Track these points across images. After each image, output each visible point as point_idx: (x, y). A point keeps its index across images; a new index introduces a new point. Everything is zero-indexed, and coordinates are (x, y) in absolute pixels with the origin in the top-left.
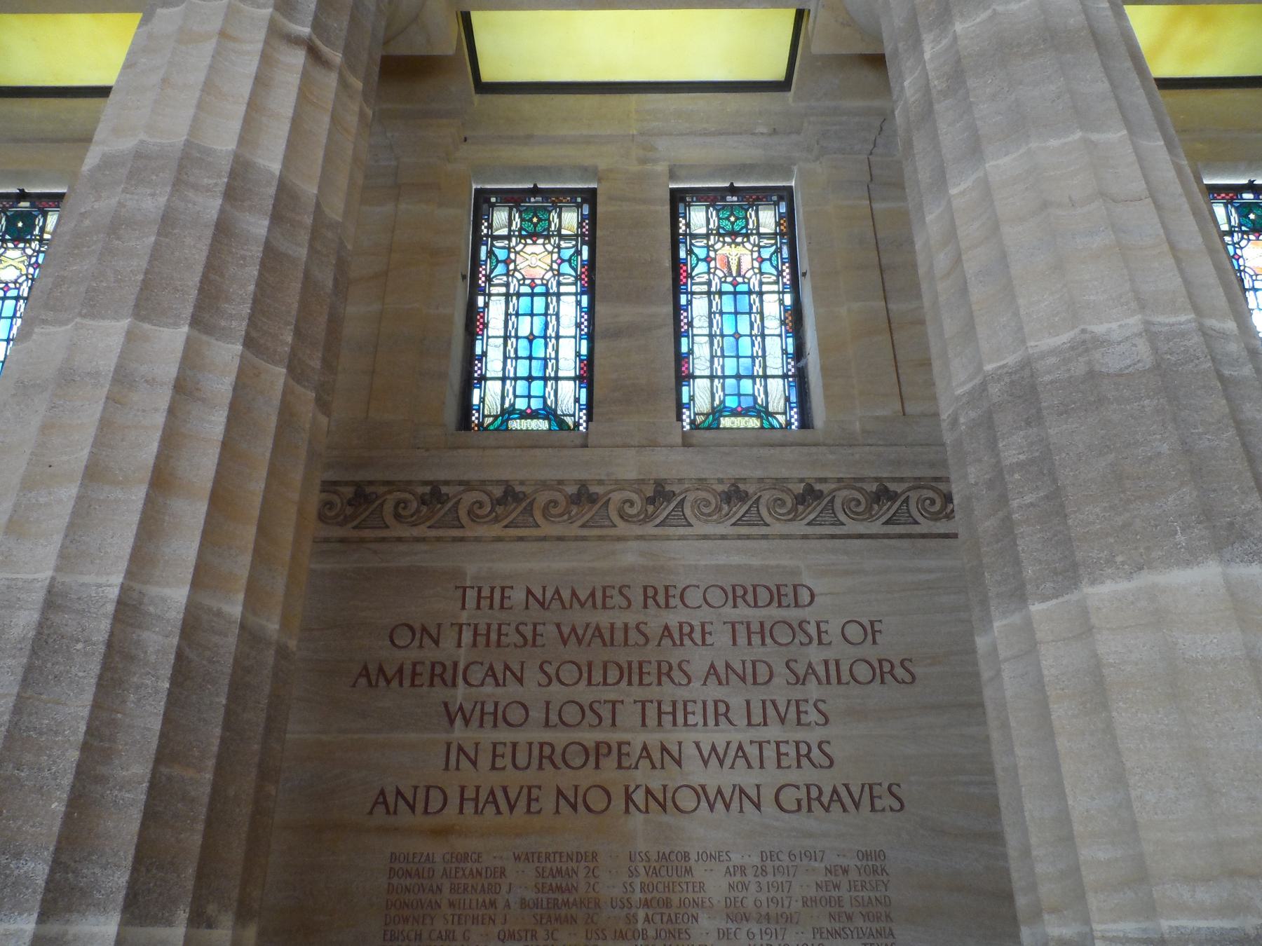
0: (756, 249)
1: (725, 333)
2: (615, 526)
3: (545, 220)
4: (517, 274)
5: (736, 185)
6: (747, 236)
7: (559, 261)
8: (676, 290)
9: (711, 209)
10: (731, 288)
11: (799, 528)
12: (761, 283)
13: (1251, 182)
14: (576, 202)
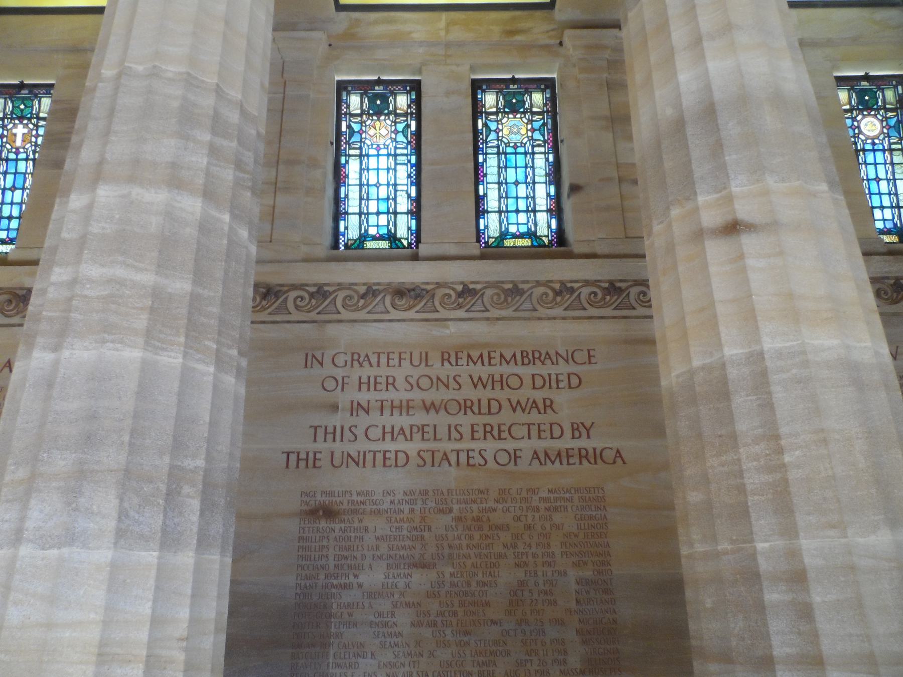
0: (393, 124)
1: (870, 178)
2: (438, 311)
3: (29, 107)
4: (861, 136)
5: (382, 78)
6: (30, 119)
7: (361, 132)
8: (476, 150)
9: (852, 91)
10: (375, 152)
11: (558, 311)
12: (396, 148)
13: (867, 74)
14: (406, 90)
